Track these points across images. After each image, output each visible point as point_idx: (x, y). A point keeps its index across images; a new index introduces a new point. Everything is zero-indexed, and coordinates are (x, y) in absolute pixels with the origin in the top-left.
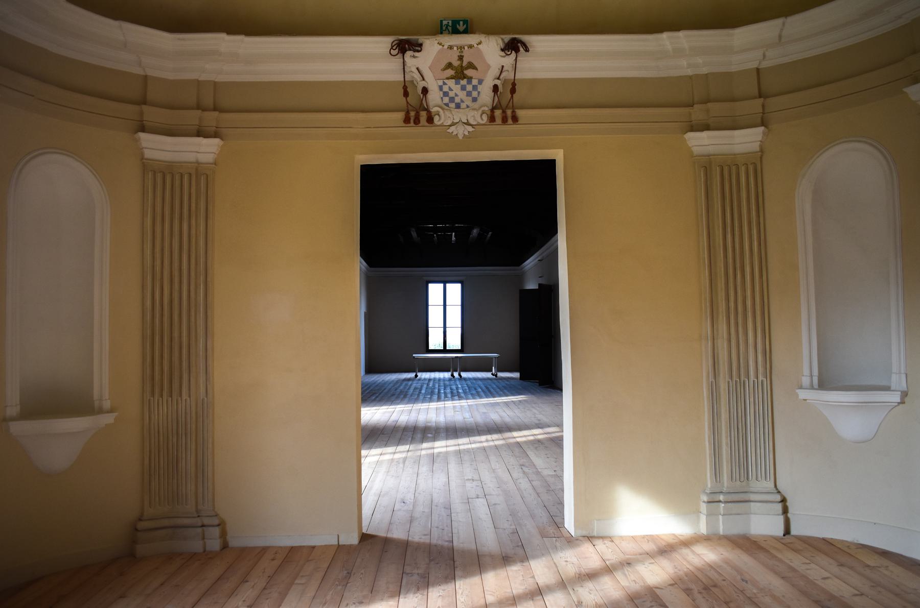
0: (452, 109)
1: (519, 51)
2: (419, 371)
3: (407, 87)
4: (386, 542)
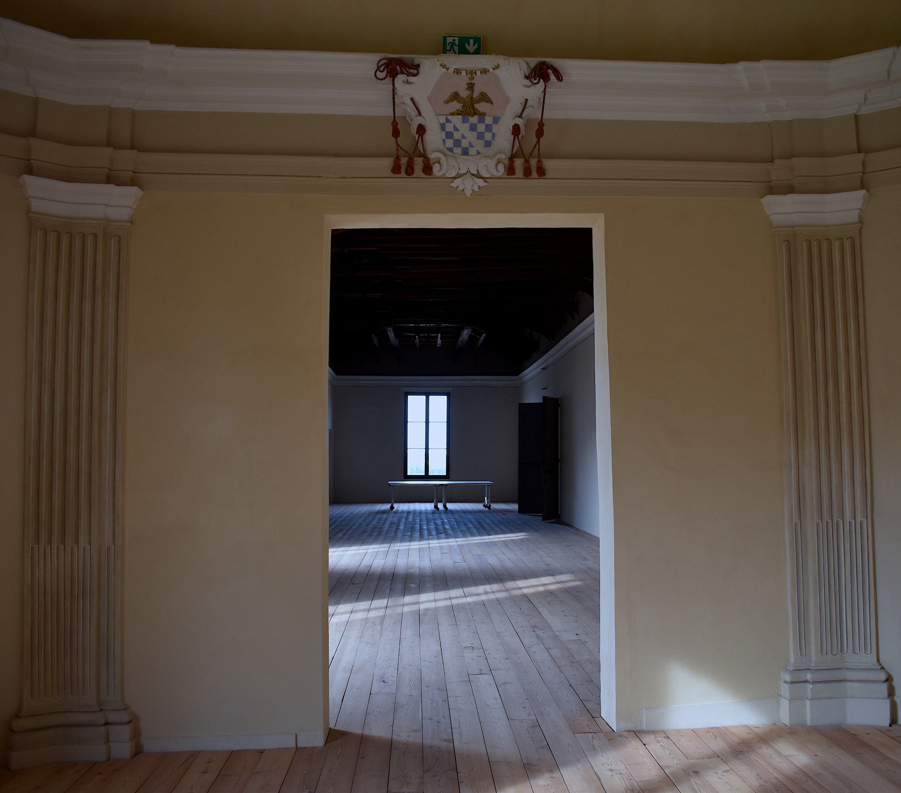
0: (456, 155)
1: (549, 80)
2: (396, 502)
3: (397, 124)
4: (363, 741)
